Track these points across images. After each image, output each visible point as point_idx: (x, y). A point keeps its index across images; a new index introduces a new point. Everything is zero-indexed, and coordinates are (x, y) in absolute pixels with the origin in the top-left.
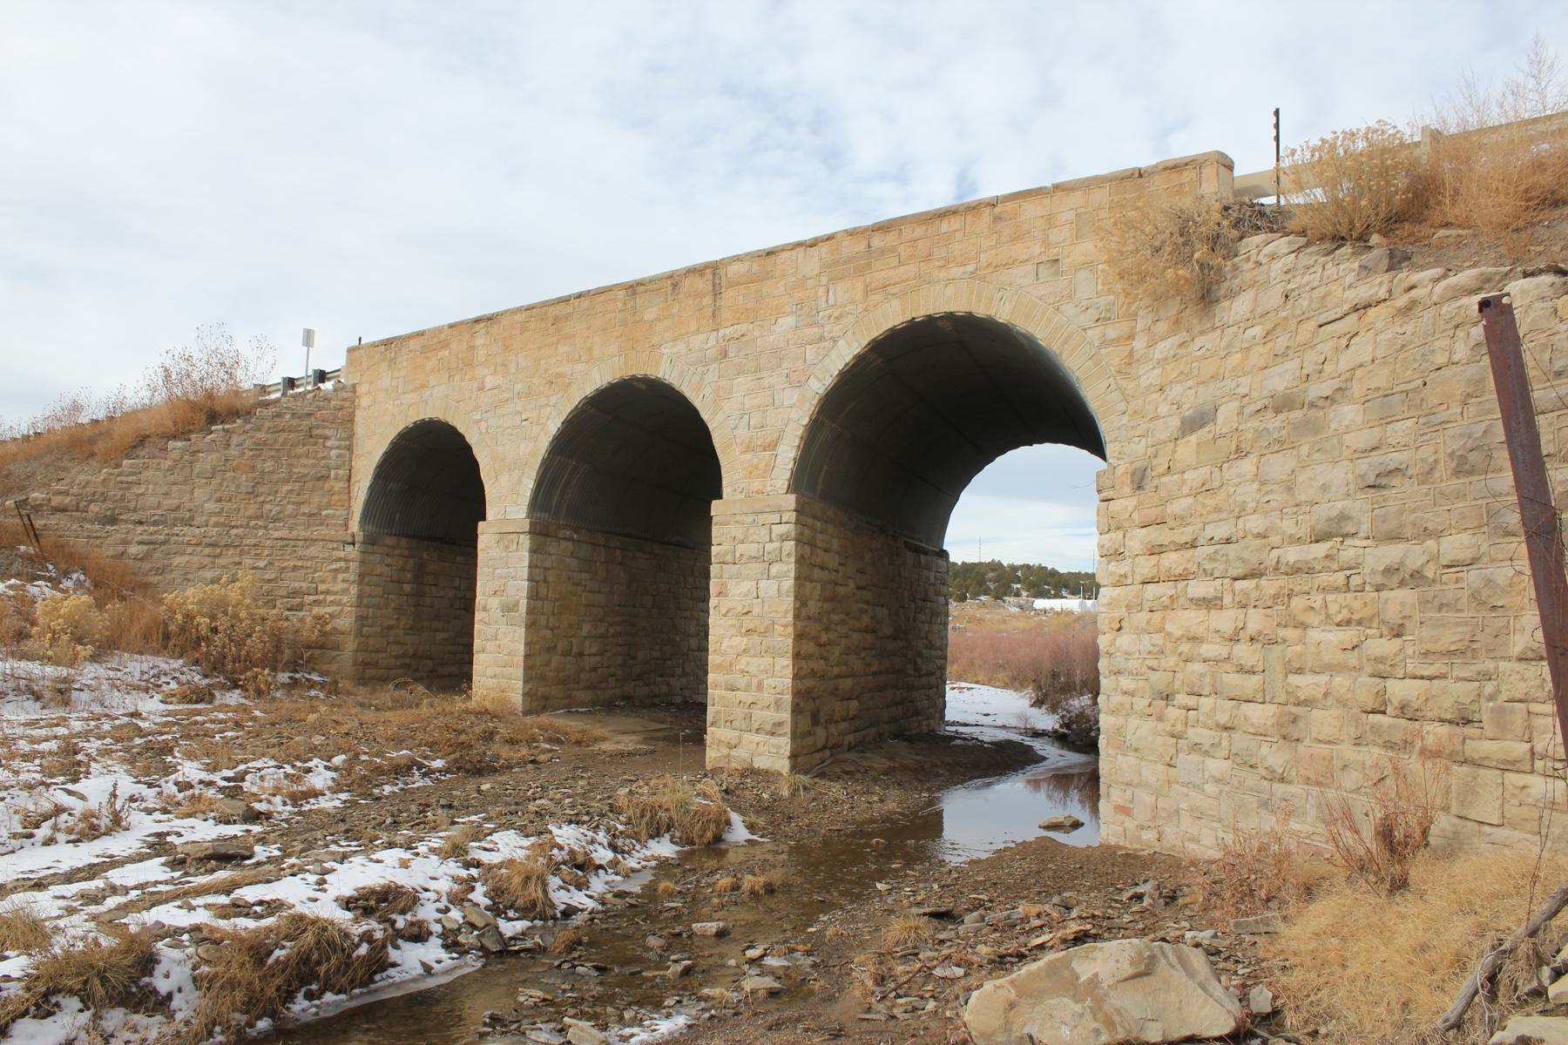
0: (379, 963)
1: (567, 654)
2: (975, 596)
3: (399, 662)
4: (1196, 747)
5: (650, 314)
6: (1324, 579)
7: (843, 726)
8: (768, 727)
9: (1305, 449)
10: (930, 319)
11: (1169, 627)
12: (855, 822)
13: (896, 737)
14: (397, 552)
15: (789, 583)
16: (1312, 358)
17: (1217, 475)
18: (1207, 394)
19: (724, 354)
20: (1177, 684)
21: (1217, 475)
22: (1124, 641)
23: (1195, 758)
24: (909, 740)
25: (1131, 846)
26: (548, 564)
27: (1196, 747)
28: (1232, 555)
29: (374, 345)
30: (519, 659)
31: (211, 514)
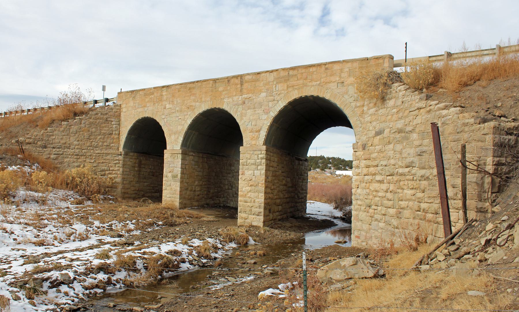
0: (178, 267)
1: (191, 191)
2: (314, 169)
3: (134, 192)
4: (376, 220)
5: (221, 89)
6: (408, 177)
7: (277, 213)
8: (257, 214)
9: (405, 144)
10: (306, 96)
11: (370, 188)
12: (283, 240)
13: (292, 217)
14: (134, 157)
15: (263, 172)
16: (407, 120)
17: (384, 148)
18: (382, 125)
19: (244, 103)
20: (372, 203)
21: (384, 148)
22: (359, 191)
23: (376, 223)
24: (296, 218)
25: (359, 247)
26: (186, 163)
27: (376, 220)
28: (387, 170)
29: (127, 92)
30: (178, 192)
31: (76, 145)
